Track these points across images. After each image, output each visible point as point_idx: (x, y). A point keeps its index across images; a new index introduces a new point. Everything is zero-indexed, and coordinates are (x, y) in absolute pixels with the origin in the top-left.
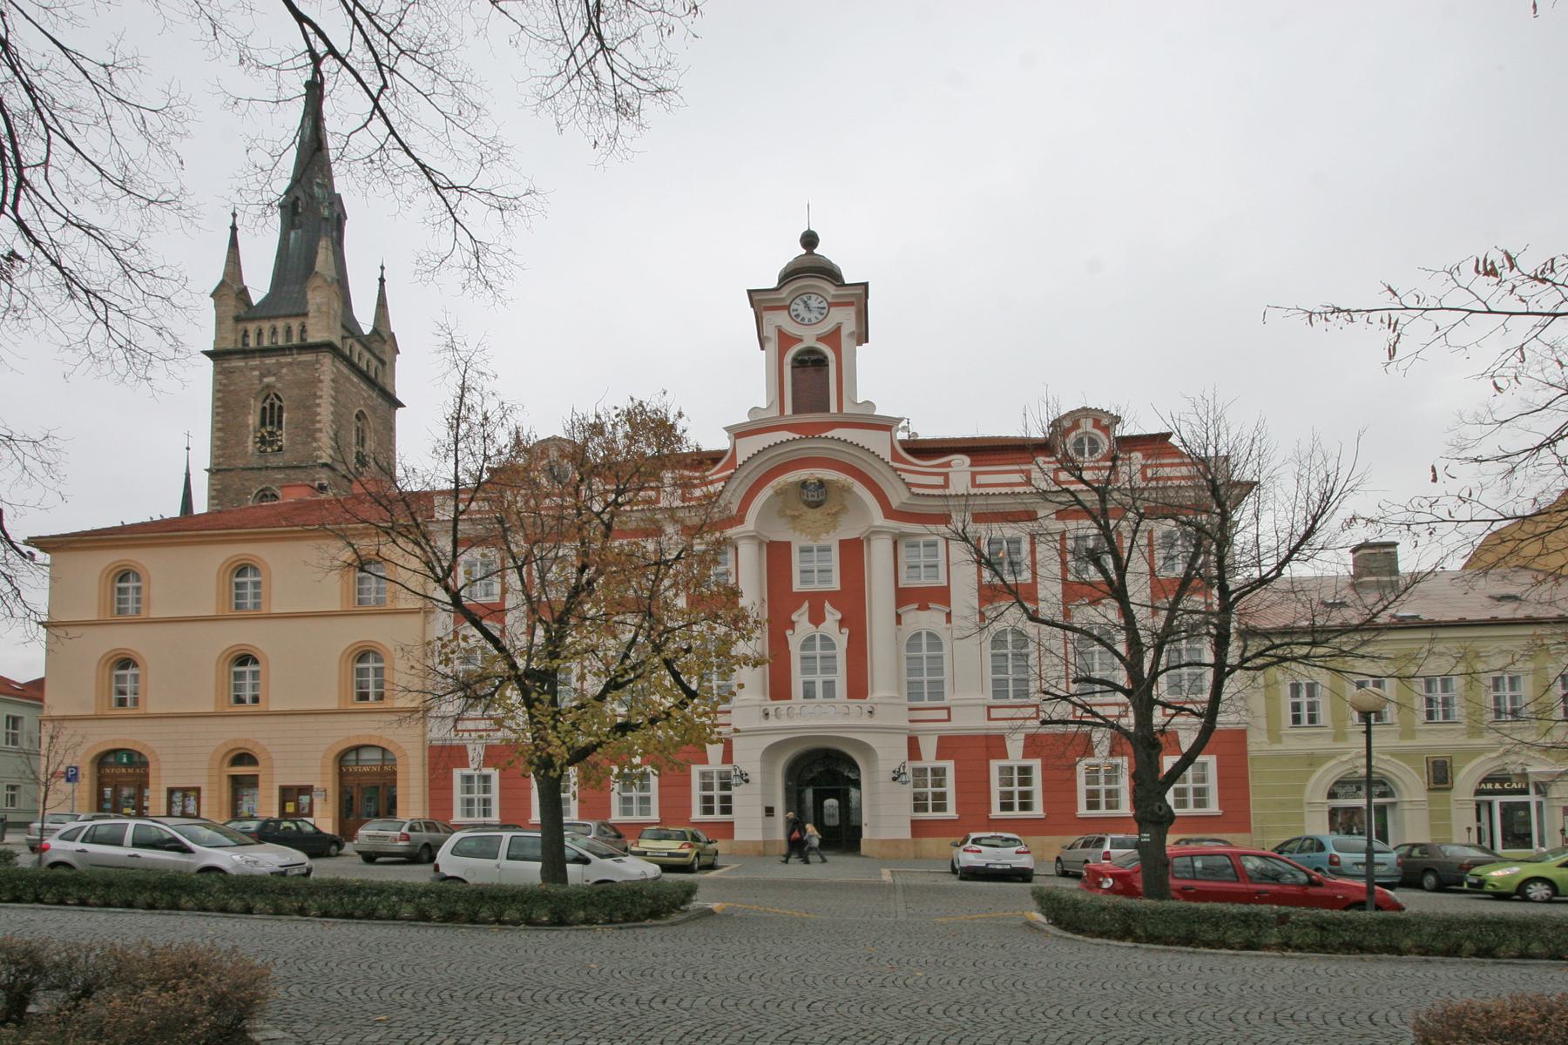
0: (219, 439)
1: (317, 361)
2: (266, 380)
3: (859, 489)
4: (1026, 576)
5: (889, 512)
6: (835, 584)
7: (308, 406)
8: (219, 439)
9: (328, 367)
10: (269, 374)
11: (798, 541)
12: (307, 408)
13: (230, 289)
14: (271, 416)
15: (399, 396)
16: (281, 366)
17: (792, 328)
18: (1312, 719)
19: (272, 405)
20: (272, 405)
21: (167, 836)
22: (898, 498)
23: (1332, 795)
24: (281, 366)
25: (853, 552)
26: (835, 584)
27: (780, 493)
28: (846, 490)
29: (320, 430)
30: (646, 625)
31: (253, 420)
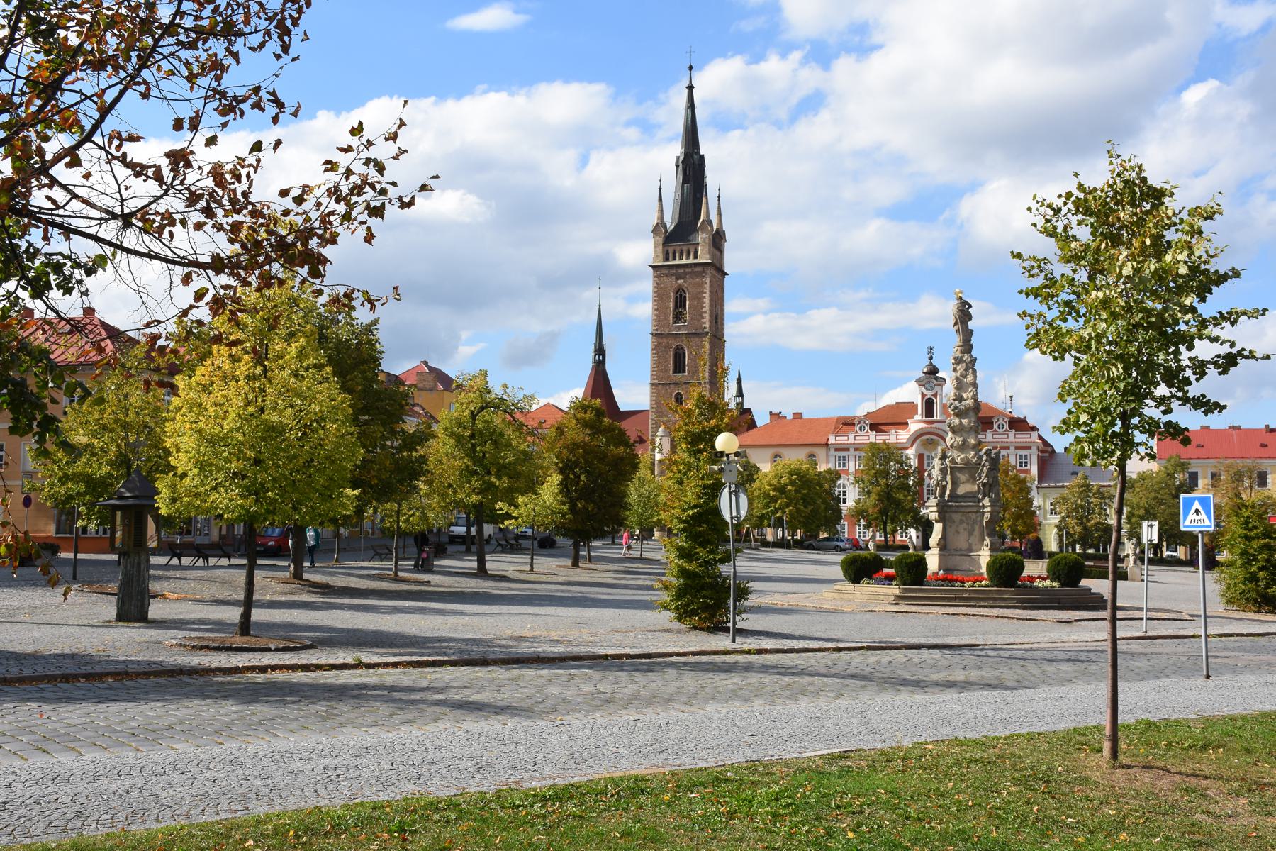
7: (698, 298)
11: (926, 453)
13: (659, 227)
14: (680, 302)
16: (686, 273)
17: (925, 392)
24: (686, 273)
31: (671, 305)
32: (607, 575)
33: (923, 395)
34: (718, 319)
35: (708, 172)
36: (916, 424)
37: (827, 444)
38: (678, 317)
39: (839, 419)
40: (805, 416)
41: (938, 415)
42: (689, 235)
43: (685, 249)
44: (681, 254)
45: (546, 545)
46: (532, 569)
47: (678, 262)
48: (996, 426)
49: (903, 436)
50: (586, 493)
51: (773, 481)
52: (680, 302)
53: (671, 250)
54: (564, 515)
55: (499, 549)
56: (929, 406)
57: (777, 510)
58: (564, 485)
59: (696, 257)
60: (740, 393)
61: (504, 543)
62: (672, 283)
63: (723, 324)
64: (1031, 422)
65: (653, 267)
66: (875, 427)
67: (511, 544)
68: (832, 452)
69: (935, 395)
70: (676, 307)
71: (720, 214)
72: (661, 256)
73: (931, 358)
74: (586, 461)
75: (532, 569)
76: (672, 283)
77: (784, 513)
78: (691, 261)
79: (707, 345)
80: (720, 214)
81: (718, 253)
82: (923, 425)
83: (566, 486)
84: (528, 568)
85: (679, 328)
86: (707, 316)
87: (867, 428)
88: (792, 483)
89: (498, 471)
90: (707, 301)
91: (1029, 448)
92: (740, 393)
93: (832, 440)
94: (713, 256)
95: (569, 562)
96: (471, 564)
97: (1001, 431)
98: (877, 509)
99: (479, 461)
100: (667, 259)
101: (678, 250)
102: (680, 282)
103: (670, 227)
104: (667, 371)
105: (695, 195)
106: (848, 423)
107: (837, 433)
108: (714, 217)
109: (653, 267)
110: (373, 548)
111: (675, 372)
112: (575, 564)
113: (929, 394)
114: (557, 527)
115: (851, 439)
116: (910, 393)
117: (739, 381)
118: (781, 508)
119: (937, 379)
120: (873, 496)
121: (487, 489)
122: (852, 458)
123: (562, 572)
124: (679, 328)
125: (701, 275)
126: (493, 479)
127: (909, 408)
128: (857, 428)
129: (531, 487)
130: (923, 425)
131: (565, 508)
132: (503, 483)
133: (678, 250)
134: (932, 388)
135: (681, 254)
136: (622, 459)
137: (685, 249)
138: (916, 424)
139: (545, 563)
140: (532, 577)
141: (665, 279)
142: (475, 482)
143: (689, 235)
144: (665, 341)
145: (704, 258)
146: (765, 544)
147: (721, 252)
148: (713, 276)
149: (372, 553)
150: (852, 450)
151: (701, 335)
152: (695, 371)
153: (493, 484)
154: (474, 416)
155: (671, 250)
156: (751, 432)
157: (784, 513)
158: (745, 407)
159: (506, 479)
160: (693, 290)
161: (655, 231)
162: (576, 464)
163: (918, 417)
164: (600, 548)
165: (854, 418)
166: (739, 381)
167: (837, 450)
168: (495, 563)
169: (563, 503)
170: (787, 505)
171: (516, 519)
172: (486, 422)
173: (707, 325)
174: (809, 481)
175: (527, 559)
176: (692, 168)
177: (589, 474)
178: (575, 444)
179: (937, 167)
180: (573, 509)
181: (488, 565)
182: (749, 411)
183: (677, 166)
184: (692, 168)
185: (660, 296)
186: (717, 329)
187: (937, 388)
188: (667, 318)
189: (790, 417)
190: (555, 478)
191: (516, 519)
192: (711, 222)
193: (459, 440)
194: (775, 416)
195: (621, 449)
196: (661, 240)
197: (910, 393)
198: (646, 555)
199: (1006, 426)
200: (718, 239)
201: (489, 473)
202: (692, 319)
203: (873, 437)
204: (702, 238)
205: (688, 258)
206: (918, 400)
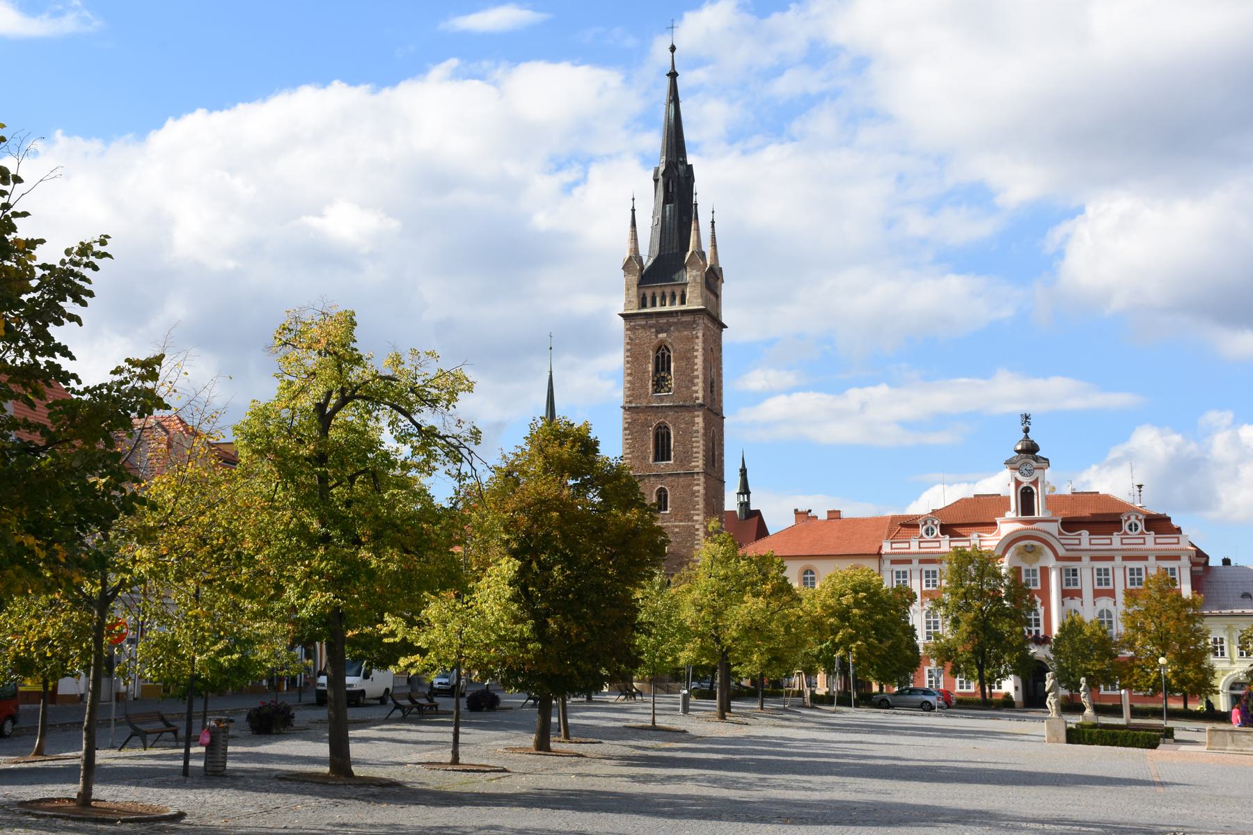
0: (629, 382)
1: (694, 322)
2: (660, 336)
3: (1047, 549)
4: (1111, 587)
5: (1058, 558)
6: (1039, 587)
7: (688, 358)
8: (629, 382)
9: (702, 321)
10: (662, 331)
11: (1024, 566)
12: (688, 359)
13: (632, 262)
14: (662, 364)
15: (724, 321)
16: (670, 324)
18: (1222, 654)
19: (663, 354)
20: (663, 354)
21: (608, 695)
22: (1062, 552)
23: (1232, 688)
24: (670, 324)
25: (1045, 572)
26: (1039, 587)
27: (1018, 548)
28: (1041, 549)
29: (697, 377)
30: (21, 344)
31: (651, 368)
32: (610, 768)
33: (1018, 483)
34: (714, 386)
35: (698, 186)
36: (1008, 525)
37: (879, 555)
38: (659, 384)
39: (894, 519)
40: (843, 515)
41: (1040, 511)
42: (674, 268)
43: (668, 291)
44: (663, 298)
45: (482, 705)
46: (455, 760)
47: (658, 309)
48: (1125, 527)
49: (990, 542)
50: (562, 602)
51: (831, 602)
52: (662, 364)
53: (649, 293)
54: (523, 642)
55: (398, 713)
56: (1026, 499)
57: (836, 647)
58: (521, 581)
59: (683, 302)
60: (745, 490)
61: (406, 702)
62: (651, 339)
63: (720, 394)
64: (1175, 522)
65: (624, 316)
66: (946, 529)
67: (414, 704)
68: (887, 565)
69: (1035, 483)
70: (657, 370)
71: (714, 245)
72: (635, 301)
73: (1027, 430)
74: (565, 537)
75: (455, 760)
76: (651, 339)
77: (848, 650)
78: (677, 307)
79: (699, 420)
80: (714, 245)
81: (712, 297)
82: (1019, 526)
83: (524, 588)
84: (447, 756)
85: (661, 399)
86: (699, 382)
87: (937, 531)
88: (857, 603)
89: (377, 536)
90: (699, 361)
91: (1178, 558)
92: (745, 490)
93: (886, 548)
94: (706, 301)
95: (530, 740)
96: (310, 751)
97: (1133, 534)
98: (969, 647)
99: (330, 517)
100: (644, 305)
101: (658, 292)
102: (662, 336)
103: (647, 262)
104: (645, 458)
105: (680, 220)
106: (910, 524)
107: (893, 538)
108: (707, 247)
109: (624, 316)
110: (129, 720)
111: (656, 459)
112: (543, 745)
113: (1026, 481)
114: (510, 672)
115: (915, 547)
116: (1002, 483)
117: (744, 472)
118: (844, 643)
119: (1037, 459)
120: (963, 626)
121: (346, 577)
122: (916, 574)
123: (519, 762)
124: (661, 399)
125: (691, 326)
126: (364, 554)
127: (999, 503)
128: (922, 531)
129: (456, 581)
130: (1019, 526)
131: (526, 629)
132: (388, 562)
133: (658, 292)
134: (1030, 473)
135: (663, 298)
136: (635, 532)
137: (668, 291)
138: (1008, 525)
139: (486, 744)
140: (455, 782)
141: (640, 333)
142: (320, 560)
143: (674, 268)
144: (642, 416)
145: (694, 301)
146: (817, 700)
147: (717, 296)
148: (706, 327)
149: (128, 731)
150: (915, 563)
151: (689, 408)
152: (687, 457)
153: (366, 563)
154: (323, 416)
155: (649, 293)
156: (760, 542)
157: (848, 650)
158: (752, 508)
159: (393, 552)
160: (680, 346)
161: (627, 267)
162: (546, 542)
163: (1011, 514)
164: (607, 710)
165: (917, 517)
166: (744, 472)
167: (893, 562)
168: (378, 749)
169: (517, 620)
170: (853, 639)
171: (423, 652)
172: (350, 428)
173: (700, 395)
174: (881, 601)
175: (446, 734)
176: (676, 184)
177: (570, 562)
178: (542, 502)
179: (1020, 182)
180: (540, 629)
181: (356, 750)
182: (758, 513)
183: (656, 181)
184: (676, 184)
185: (634, 356)
186: (713, 400)
187: (1037, 473)
188: (644, 386)
189: (823, 516)
190: (508, 567)
191: (423, 652)
192: (703, 254)
193: (287, 467)
194: (803, 516)
195: (633, 514)
196: (635, 279)
197: (1002, 483)
198: (662, 721)
199: (1141, 527)
200: (713, 279)
201: (357, 542)
202: (679, 387)
203: (946, 545)
204: (691, 276)
205: (672, 303)
206: (1011, 492)
